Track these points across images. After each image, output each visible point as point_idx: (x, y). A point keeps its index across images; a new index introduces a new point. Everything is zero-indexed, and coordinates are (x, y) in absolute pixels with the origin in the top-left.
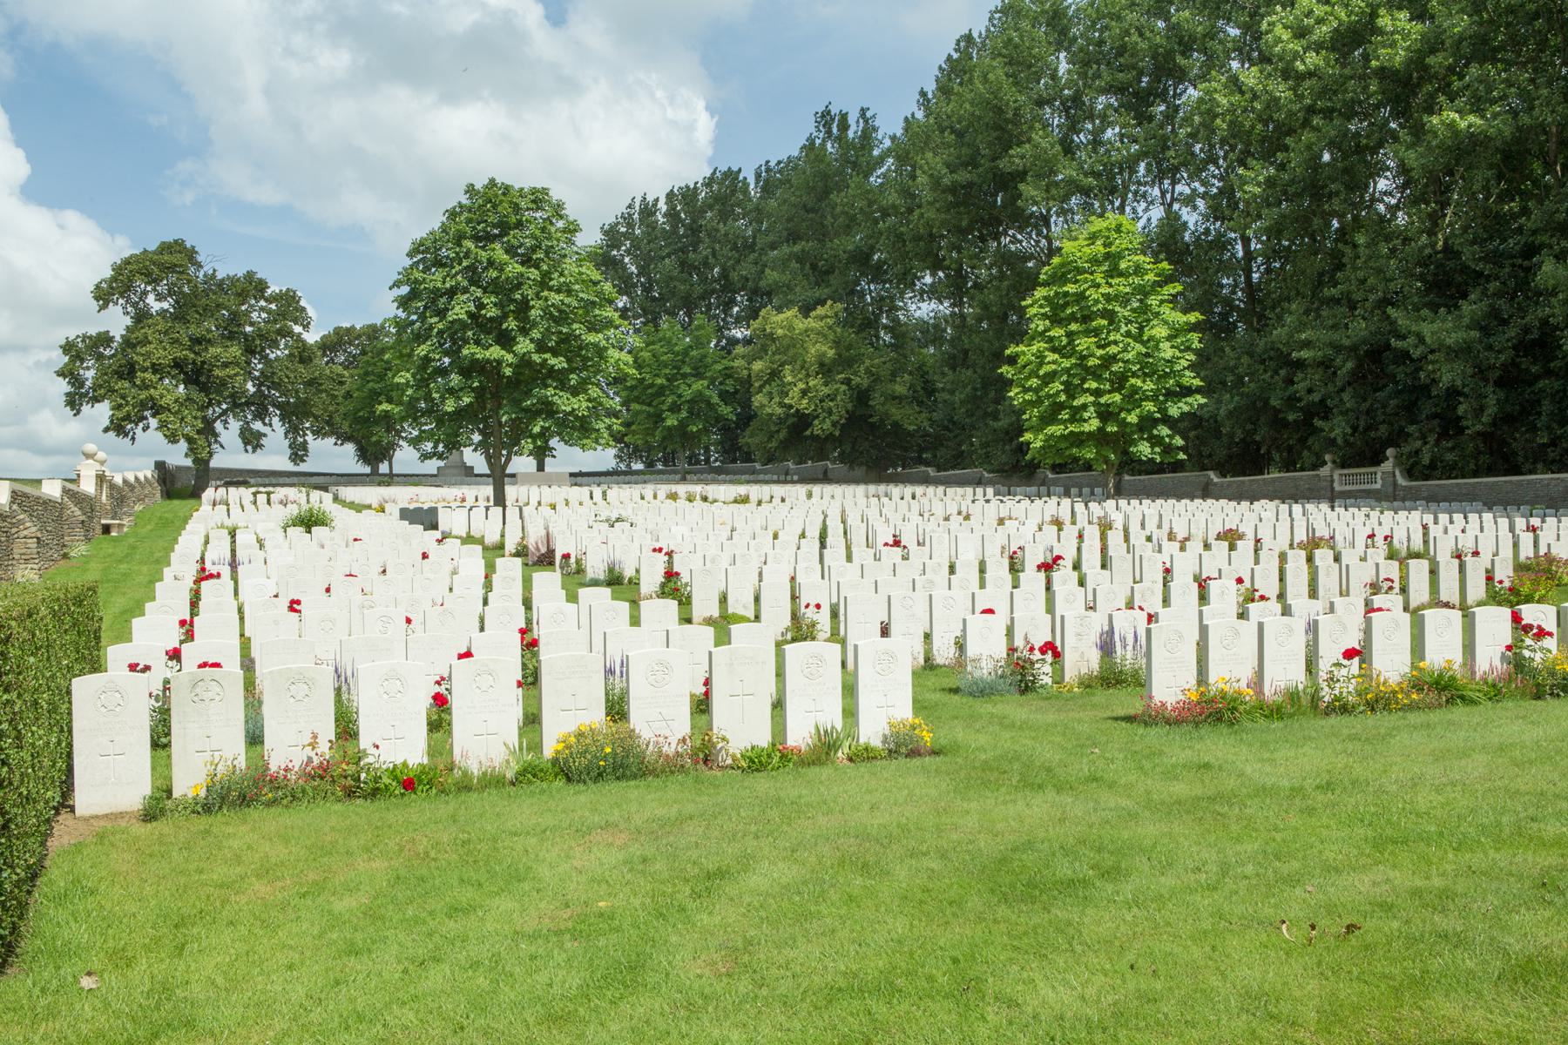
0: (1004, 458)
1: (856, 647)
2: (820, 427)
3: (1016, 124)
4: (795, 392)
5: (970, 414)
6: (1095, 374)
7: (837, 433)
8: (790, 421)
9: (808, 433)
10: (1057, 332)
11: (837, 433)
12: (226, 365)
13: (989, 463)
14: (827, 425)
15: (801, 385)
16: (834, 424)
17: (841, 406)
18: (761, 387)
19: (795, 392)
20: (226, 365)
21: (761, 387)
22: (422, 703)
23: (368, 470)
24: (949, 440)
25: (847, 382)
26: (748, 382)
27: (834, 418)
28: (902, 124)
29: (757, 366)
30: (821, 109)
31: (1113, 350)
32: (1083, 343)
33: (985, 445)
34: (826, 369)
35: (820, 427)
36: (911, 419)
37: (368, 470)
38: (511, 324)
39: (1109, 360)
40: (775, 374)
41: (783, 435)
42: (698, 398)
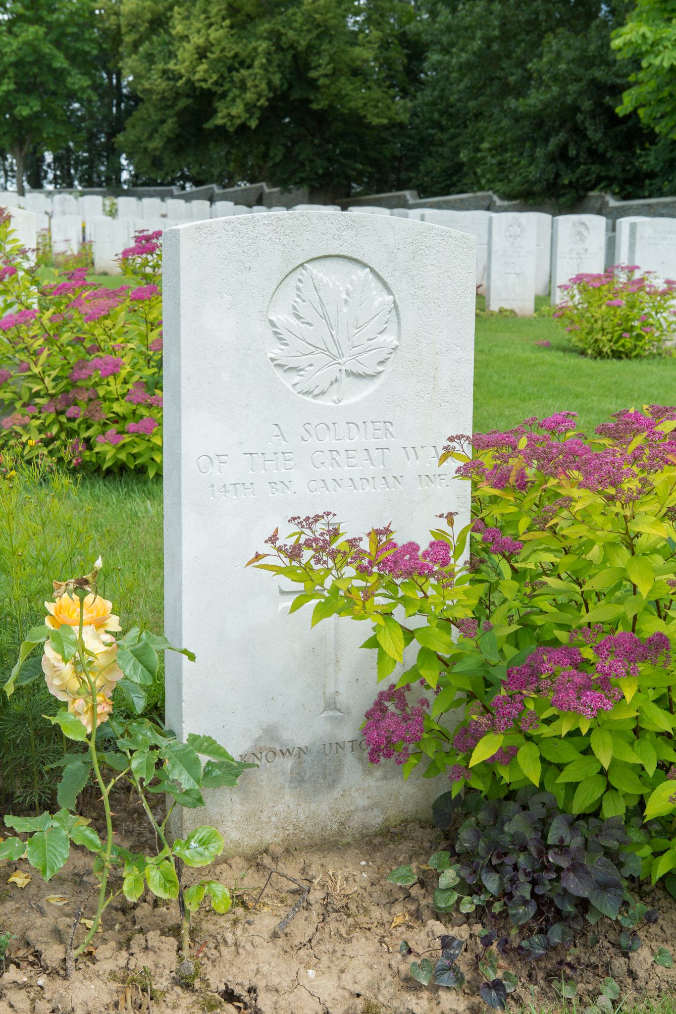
0: (534, 172)
2: (231, 112)
3: (159, 802)
4: (186, 53)
5: (474, 92)
7: (253, 124)
8: (183, 103)
9: (209, 125)
11: (253, 124)
13: (506, 180)
14: (238, 109)
15: (198, 40)
16: (250, 108)
17: (257, 83)
18: (136, 45)
19: (186, 53)
21: (136, 45)
24: (442, 144)
27: (249, 96)
28: (624, 811)
33: (500, 148)
35: (231, 112)
36: (378, 105)
41: (169, 127)
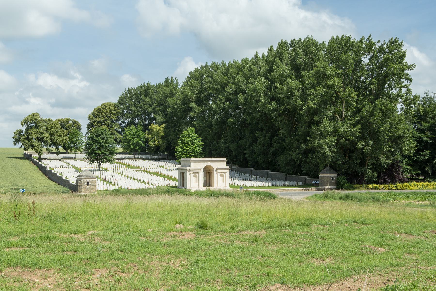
1: (272, 196)
6: (186, 152)
10: (181, 145)
12: (47, 138)
14: (162, 149)
16: (164, 149)
20: (47, 138)
22: (369, 35)
23: (65, 151)
25: (167, 140)
26: (148, 139)
29: (150, 136)
30: (166, 77)
31: (188, 149)
32: (184, 147)
34: (163, 138)
37: (65, 151)
38: (101, 148)
39: (187, 150)
40: (153, 138)
42: (137, 142)
